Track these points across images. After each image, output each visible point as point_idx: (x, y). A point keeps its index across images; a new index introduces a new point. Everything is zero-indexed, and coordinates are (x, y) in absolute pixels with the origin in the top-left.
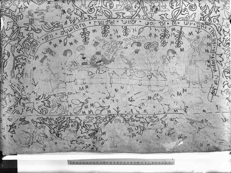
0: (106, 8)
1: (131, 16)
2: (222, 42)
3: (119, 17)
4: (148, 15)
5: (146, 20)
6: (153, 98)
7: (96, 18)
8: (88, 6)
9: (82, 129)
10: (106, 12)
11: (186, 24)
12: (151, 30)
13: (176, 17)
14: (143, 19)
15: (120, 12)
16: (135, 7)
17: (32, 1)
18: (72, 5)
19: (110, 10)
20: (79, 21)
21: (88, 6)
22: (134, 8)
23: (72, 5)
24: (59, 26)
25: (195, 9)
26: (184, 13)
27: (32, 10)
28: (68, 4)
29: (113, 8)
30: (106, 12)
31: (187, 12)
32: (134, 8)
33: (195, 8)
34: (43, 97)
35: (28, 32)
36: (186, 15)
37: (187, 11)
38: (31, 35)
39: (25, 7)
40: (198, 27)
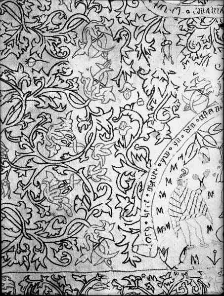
0: (138, 191)
5: (23, 197)
6: (51, 122)
8: (147, 245)
10: (70, 25)
13: (86, 14)
16: (66, 174)
17: (38, 1)
18: (100, 122)
20: (49, 157)
21: (147, 245)
22: (67, 177)
23: (100, 122)
24: (51, 141)
26: (76, 85)
28: (136, 39)
29: (66, 11)
30: (70, 25)
31: (79, 172)
32: (67, 177)
34: (66, 26)
36: (79, 82)
37: (72, 80)
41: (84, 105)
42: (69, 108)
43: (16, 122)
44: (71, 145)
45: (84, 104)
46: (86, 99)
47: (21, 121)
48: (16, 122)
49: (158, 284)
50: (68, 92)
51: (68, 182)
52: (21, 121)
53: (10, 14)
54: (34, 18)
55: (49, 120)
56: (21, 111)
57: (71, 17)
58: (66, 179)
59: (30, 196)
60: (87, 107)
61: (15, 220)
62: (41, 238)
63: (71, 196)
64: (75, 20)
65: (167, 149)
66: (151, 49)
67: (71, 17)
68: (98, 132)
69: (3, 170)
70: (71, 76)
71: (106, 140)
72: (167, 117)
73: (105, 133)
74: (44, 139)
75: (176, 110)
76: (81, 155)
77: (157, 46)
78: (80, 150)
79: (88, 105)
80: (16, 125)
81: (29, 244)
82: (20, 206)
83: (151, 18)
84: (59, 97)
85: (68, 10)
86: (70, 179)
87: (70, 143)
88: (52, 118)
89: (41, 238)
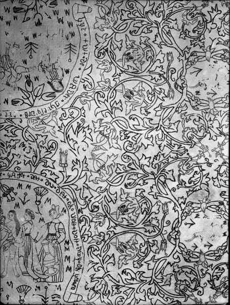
6: (141, 107)
41: (117, 119)
42: (127, 117)
43: (159, 261)
44: (120, 244)
45: (117, 120)
46: (114, 124)
48: (159, 261)
50: (129, 129)
51: (121, 213)
54: (160, 89)
55: (136, 263)
56: (156, 269)
59: (155, 52)
60: (106, 271)
64: (124, 123)
71: (94, 246)
72: (71, 111)
73: (94, 251)
74: (139, 248)
75: (63, 114)
77: (70, 165)
79: (106, 273)
80: (159, 259)
81: (156, 18)
83: (73, 153)
84: (135, 126)
88: (133, 265)
89: (137, 230)
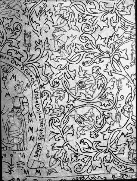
1: (70, 88)
2: (60, 121)
3: (83, 16)
4: (74, 111)
5: (79, 30)
7: (123, 3)
9: (104, 27)
11: (8, 115)
12: (104, 26)
14: (7, 147)
15: (85, 54)
19: (81, 62)
23: (24, 163)
25: (76, 171)
27: (52, 34)
33: (76, 171)
35: (96, 140)
38: (93, 135)
39: (68, 39)
40: (63, 55)
44: (78, 116)
47: (111, 133)
49: (60, 100)
51: (79, 89)
52: (111, 133)
53: (126, 123)
57: (35, 66)
58: (81, 91)
61: (122, 160)
62: (95, 104)
63: (78, 79)
65: (31, 74)
66: (25, 12)
67: (35, 66)
68: (59, 124)
69: (135, 174)
70: (63, 88)
76: (72, 109)
78: (73, 113)
80: (113, 130)
82: (121, 168)
85: (35, 48)
86: (78, 90)
87: (78, 117)
